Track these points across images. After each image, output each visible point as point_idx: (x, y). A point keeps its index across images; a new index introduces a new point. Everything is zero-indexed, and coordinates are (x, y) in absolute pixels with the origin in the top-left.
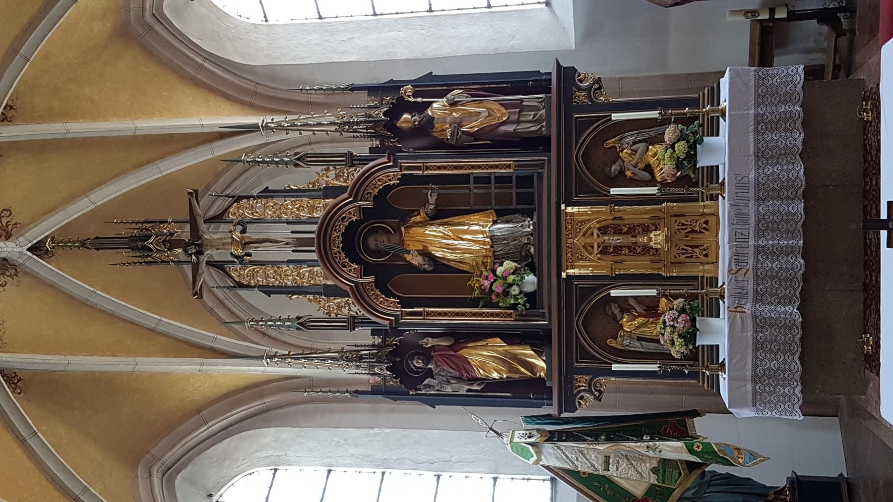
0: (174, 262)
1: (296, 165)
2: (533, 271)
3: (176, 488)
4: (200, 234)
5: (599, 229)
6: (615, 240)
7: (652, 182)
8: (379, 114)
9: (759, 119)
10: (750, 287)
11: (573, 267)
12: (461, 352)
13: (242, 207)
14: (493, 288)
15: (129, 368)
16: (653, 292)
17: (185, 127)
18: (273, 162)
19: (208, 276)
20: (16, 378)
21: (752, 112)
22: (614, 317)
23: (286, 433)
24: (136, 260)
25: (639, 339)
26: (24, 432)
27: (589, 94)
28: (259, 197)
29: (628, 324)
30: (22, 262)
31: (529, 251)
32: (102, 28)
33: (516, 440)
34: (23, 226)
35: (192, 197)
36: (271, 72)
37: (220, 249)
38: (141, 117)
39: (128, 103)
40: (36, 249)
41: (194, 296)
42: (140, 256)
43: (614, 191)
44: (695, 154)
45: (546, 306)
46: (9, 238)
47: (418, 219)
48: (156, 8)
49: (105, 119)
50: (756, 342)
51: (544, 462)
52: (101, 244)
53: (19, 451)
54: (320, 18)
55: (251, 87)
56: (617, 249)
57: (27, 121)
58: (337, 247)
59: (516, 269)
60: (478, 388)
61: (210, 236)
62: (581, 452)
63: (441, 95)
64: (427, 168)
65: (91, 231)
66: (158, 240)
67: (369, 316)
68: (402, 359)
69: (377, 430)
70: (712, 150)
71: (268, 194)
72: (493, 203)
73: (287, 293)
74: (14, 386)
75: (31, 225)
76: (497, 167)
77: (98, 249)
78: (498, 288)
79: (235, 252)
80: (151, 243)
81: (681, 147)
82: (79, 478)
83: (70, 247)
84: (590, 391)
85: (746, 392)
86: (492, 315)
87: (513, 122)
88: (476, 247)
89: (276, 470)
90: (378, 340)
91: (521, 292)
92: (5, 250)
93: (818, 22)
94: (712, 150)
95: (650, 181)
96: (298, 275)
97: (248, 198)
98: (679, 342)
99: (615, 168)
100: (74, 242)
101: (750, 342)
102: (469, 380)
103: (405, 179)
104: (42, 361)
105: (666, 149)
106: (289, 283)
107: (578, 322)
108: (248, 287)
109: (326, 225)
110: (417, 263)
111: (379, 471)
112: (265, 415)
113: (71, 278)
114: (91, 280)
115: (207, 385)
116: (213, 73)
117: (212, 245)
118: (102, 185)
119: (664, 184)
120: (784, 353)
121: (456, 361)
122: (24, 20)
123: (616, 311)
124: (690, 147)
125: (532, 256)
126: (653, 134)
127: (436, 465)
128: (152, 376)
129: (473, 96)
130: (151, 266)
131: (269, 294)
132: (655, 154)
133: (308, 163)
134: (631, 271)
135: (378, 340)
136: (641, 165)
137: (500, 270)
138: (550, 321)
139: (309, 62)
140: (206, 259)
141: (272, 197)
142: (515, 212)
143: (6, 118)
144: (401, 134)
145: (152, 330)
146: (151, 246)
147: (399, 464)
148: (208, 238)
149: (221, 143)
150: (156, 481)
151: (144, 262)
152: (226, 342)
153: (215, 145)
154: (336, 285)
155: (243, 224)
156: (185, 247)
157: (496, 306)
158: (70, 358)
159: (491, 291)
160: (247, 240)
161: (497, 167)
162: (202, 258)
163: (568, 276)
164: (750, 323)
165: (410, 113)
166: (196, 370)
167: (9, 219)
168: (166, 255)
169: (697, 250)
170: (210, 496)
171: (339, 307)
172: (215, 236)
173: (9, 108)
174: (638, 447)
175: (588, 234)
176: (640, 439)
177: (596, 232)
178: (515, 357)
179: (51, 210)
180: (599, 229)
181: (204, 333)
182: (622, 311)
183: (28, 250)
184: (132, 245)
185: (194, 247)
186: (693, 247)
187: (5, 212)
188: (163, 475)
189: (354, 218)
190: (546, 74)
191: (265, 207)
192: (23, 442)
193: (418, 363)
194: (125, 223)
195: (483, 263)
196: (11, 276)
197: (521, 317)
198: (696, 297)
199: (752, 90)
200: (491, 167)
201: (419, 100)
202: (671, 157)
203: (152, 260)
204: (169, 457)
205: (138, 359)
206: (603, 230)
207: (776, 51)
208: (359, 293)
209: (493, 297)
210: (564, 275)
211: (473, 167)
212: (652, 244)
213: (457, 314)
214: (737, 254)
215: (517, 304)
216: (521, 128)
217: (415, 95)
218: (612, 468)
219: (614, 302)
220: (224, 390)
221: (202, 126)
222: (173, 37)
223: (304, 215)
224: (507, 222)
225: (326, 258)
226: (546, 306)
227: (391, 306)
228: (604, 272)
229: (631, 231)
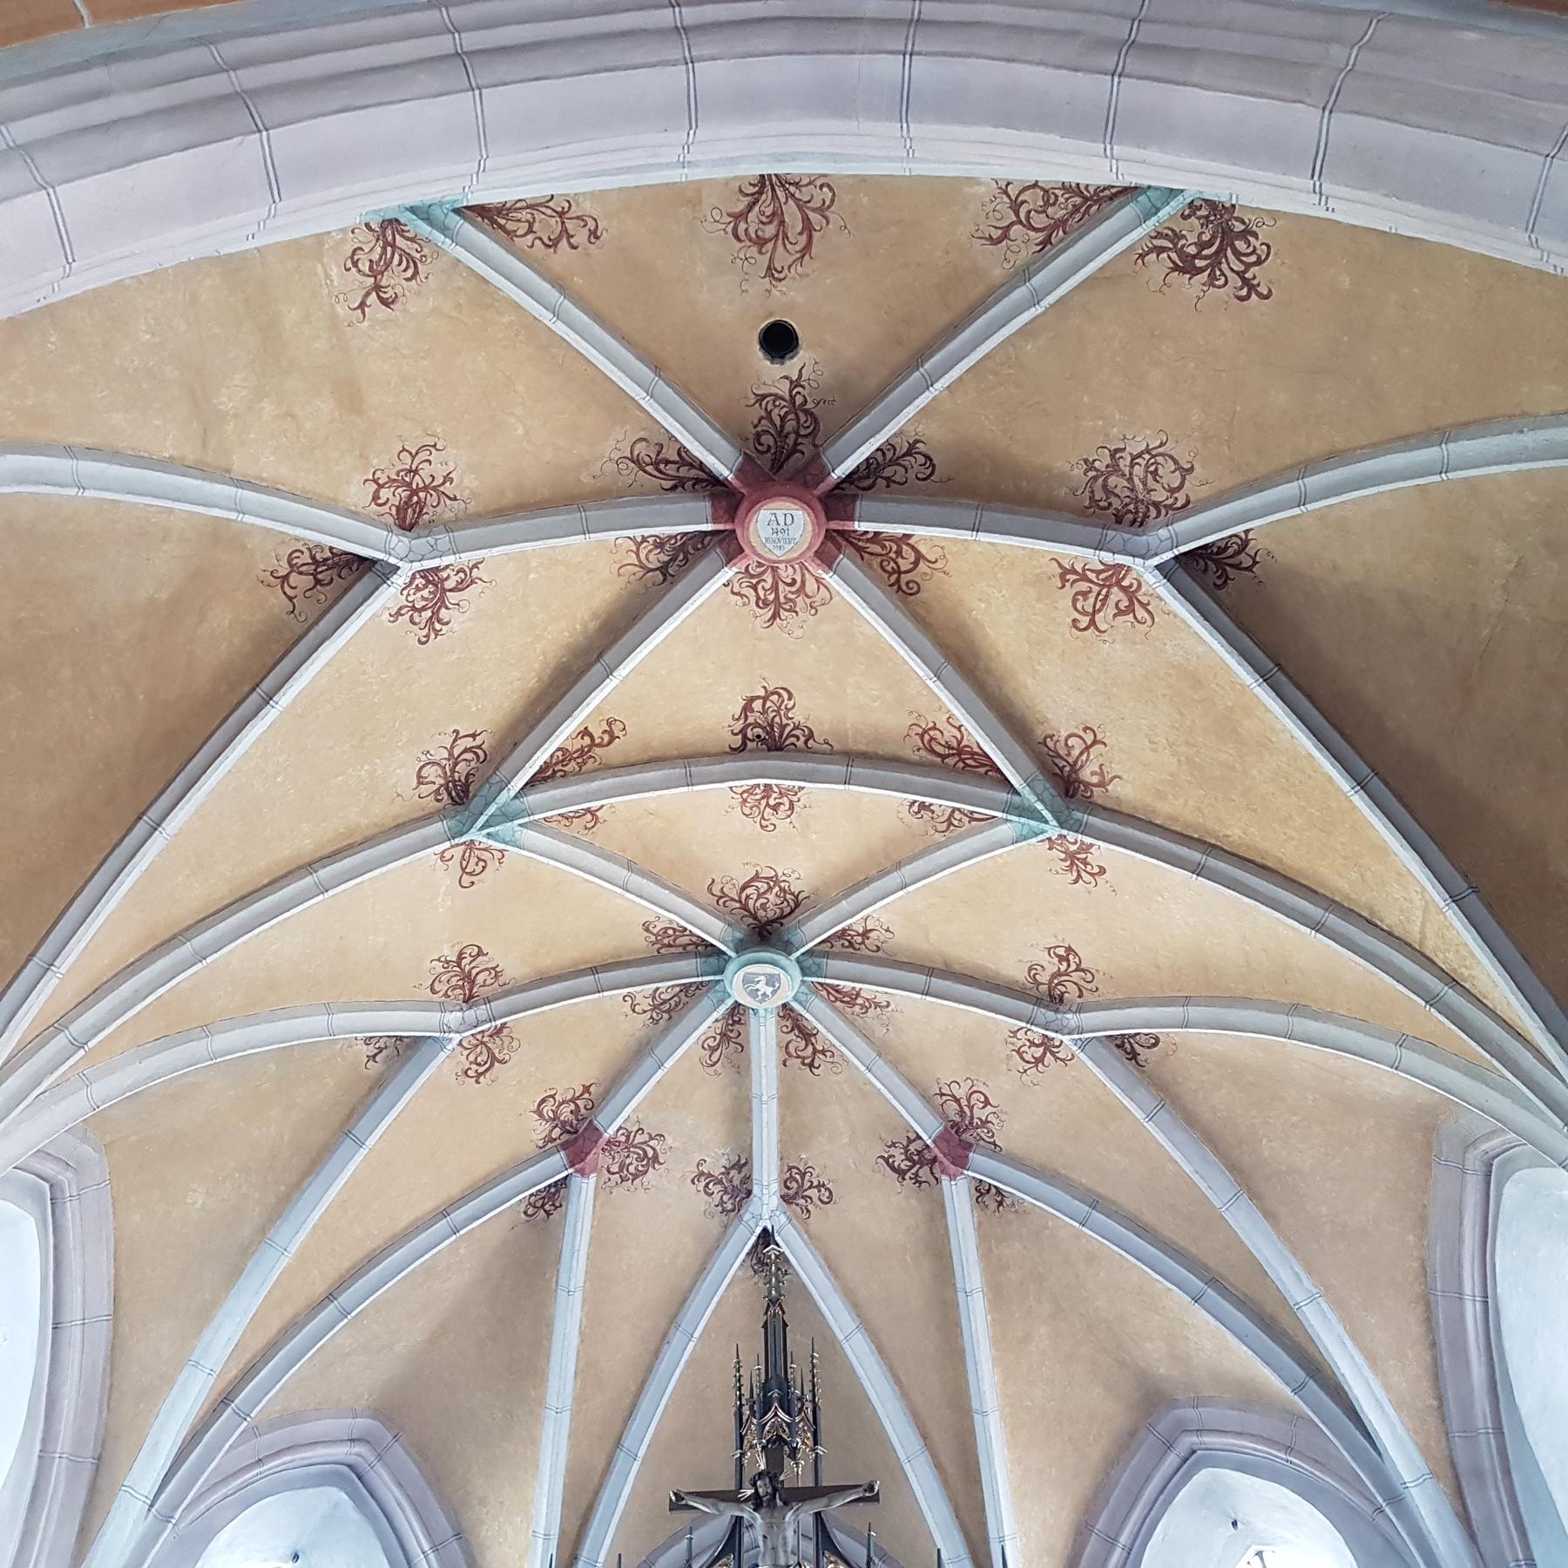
0: (740, 1458)
3: (322, 1489)
4: (794, 1504)
15: (551, 1399)
17: (993, 1478)
20: (552, 1208)
24: (745, 1391)
30: (745, 1219)
32: (1156, 1359)
34: (805, 1222)
35: (865, 1490)
37: (764, 1542)
38: (1006, 1426)
39: (1029, 1403)
41: (675, 1494)
42: (752, 1396)
46: (785, 1201)
48: (1205, 1455)
49: (997, 1361)
52: (775, 1331)
53: (428, 1205)
57: (979, 1226)
61: (789, 1523)
65: (798, 1337)
66: (782, 1427)
74: (539, 1204)
75: (806, 1236)
77: (765, 1326)
80: (776, 1415)
82: (367, 1302)
83: (770, 1282)
92: (765, 1191)
104: (577, 1248)
113: (716, 1299)
114: (713, 1335)
115: (507, 1549)
118: (880, 1353)
122: (1149, 1218)
128: (534, 1442)
130: (733, 1418)
140: (745, 1516)
143: (982, 1194)
145: (618, 1442)
146: (770, 1414)
148: (787, 1519)
150: (341, 1451)
151: (741, 1405)
156: (768, 1473)
158: (579, 1296)
162: (749, 1508)
166: (537, 1523)
167: (815, 1199)
172: (790, 1533)
173: (999, 1199)
181: (607, 1542)
184: (773, 1383)
185: (769, 1490)
187: (827, 1194)
188: (350, 1466)
194: (812, 1371)
196: (722, 1202)
203: (745, 1418)
204: (382, 1479)
205: (567, 1416)
222: (1159, 1489)
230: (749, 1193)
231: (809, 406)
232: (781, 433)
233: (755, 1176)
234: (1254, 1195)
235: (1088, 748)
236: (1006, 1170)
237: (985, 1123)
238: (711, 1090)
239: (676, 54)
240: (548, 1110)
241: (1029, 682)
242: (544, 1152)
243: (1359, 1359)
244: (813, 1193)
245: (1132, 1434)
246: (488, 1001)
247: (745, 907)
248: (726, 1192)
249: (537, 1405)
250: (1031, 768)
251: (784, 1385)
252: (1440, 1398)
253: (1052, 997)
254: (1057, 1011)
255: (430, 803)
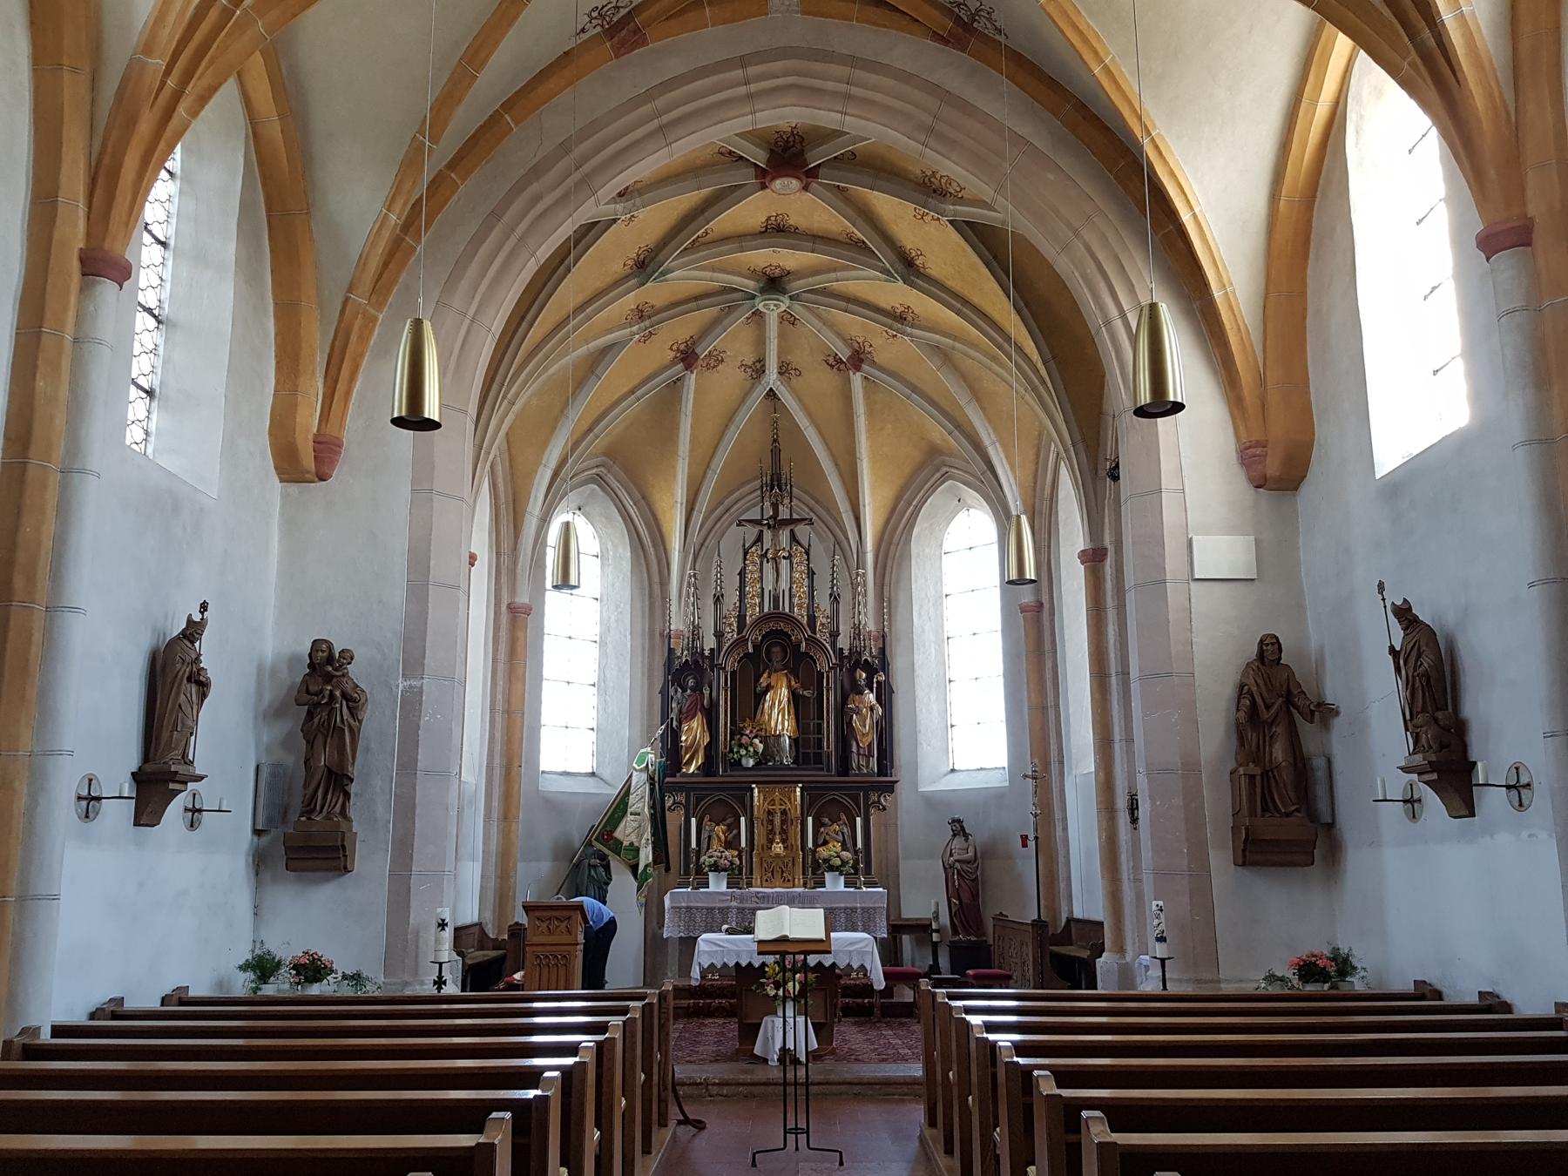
1: (831, 595)
2: (757, 764)
5: (785, 810)
6: (777, 820)
7: (816, 844)
8: (866, 656)
9: (854, 910)
10: (747, 905)
11: (759, 792)
12: (699, 713)
13: (801, 556)
14: (744, 737)
15: (681, 453)
16: (743, 844)
17: (863, 484)
18: (833, 572)
19: (752, 532)
21: (858, 905)
22: (724, 820)
23: (626, 566)
25: (709, 837)
26: (639, 393)
27: (876, 803)
28: (808, 568)
29: (720, 830)
31: (770, 761)
33: (650, 755)
36: (906, 556)
40: (771, 394)
43: (810, 819)
44: (833, 871)
45: (732, 773)
47: (793, 683)
49: (868, 438)
50: (714, 909)
51: (635, 773)
52: (776, 452)
54: (947, 596)
55: (895, 540)
56: (771, 822)
58: (772, 625)
59: (758, 753)
60: (674, 726)
62: (642, 798)
63: (878, 699)
64: (828, 691)
67: (724, 650)
68: (693, 670)
69: (629, 637)
70: (835, 881)
71: (811, 574)
72: (804, 721)
73: (740, 587)
76: (828, 739)
78: (745, 740)
79: (770, 551)
81: (838, 862)
84: (674, 803)
85: (681, 902)
86: (726, 735)
87: (858, 751)
88: (773, 724)
89: (597, 557)
90: (707, 653)
91: (741, 756)
93: (931, 965)
94: (835, 881)
95: (817, 843)
96: (753, 595)
97: (808, 560)
98: (712, 860)
99: (826, 820)
100: (777, 434)
101: (714, 905)
102: (680, 719)
103: (820, 674)
105: (836, 853)
106: (747, 589)
107: (722, 795)
108: (745, 559)
109: (789, 619)
110: (761, 681)
111: (597, 639)
112: (640, 547)
116: (905, 512)
117: (775, 537)
119: (814, 852)
120: (705, 926)
121: (694, 710)
122: (936, 398)
123: (728, 821)
124: (837, 867)
125: (766, 763)
126: (849, 845)
127: (603, 684)
129: (877, 722)
131: (740, 574)
132: (834, 846)
133: (832, 604)
134: (756, 831)
135: (707, 653)
136: (828, 838)
137: (756, 741)
138: (722, 776)
139: (913, 587)
141: (808, 577)
142: (797, 752)
144: (852, 671)
145: (708, 466)
147: (603, 655)
149: (852, 518)
150: (594, 471)
152: (698, 519)
153: (851, 513)
154: (745, 626)
155: (790, 557)
157: (731, 739)
159: (742, 735)
160: (778, 561)
161: (828, 739)
162: (766, 527)
163: (753, 789)
164: (725, 905)
165: (867, 678)
168: (767, 504)
169: (770, 874)
170: (580, 509)
171: (730, 625)
174: (648, 835)
175: (782, 802)
176: (653, 835)
177: (783, 807)
178: (696, 751)
179: (800, 400)
180: (785, 810)
182: (728, 826)
183: (771, 389)
186: (772, 872)
189: (793, 638)
190: (891, 773)
191: (801, 572)
192: (632, 392)
193: (691, 682)
195: (762, 729)
197: (725, 755)
198: (741, 873)
199: (871, 905)
200: (828, 735)
201: (875, 685)
202: (831, 856)
204: (610, 479)
205: (687, 458)
206: (784, 813)
207: (913, 936)
208: (741, 642)
209: (738, 737)
210: (754, 786)
211: (828, 723)
212: (775, 844)
213: (726, 711)
214: (768, 897)
215: (733, 753)
216: (855, 756)
217: (877, 682)
218: (632, 817)
219: (735, 820)
220: (660, 516)
221: (864, 506)
223: (796, 600)
224: (790, 745)
225: (764, 619)
226: (732, 773)
227: (731, 664)
228: (756, 813)
229: (783, 831)
230: (764, 371)
231: (800, 134)
232: (787, 141)
233: (767, 366)
234: (978, 400)
235: (918, 255)
236: (878, 373)
237: (870, 353)
238: (748, 334)
239: (748, 110)
240: (675, 347)
241: (895, 227)
242: (673, 363)
243: (1007, 467)
244: (792, 372)
245: (924, 463)
246: (649, 317)
247: (765, 274)
248: (753, 371)
249: (675, 453)
250: (893, 257)
251: (779, 480)
252: (1035, 483)
253: (901, 318)
254: (903, 324)
255: (629, 271)
